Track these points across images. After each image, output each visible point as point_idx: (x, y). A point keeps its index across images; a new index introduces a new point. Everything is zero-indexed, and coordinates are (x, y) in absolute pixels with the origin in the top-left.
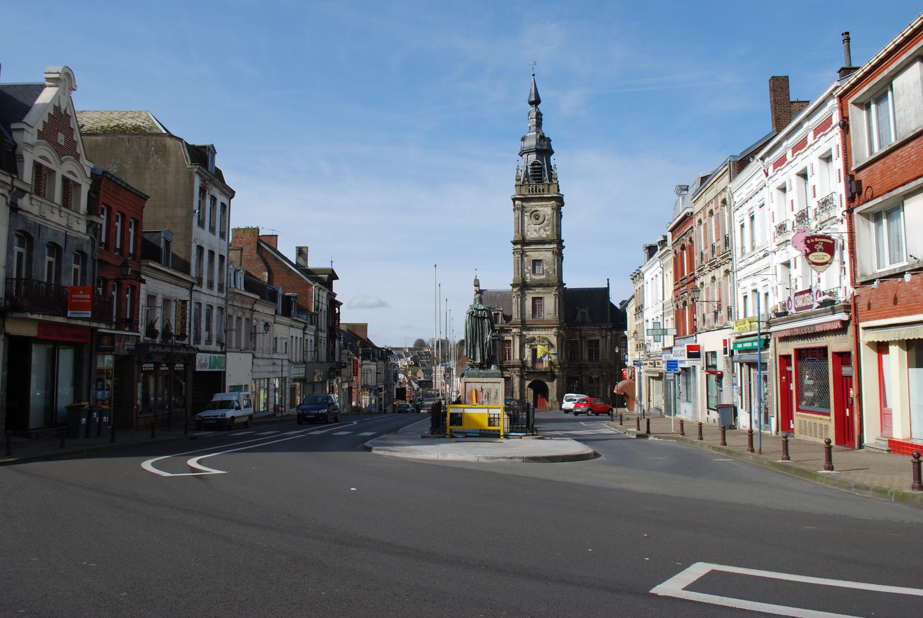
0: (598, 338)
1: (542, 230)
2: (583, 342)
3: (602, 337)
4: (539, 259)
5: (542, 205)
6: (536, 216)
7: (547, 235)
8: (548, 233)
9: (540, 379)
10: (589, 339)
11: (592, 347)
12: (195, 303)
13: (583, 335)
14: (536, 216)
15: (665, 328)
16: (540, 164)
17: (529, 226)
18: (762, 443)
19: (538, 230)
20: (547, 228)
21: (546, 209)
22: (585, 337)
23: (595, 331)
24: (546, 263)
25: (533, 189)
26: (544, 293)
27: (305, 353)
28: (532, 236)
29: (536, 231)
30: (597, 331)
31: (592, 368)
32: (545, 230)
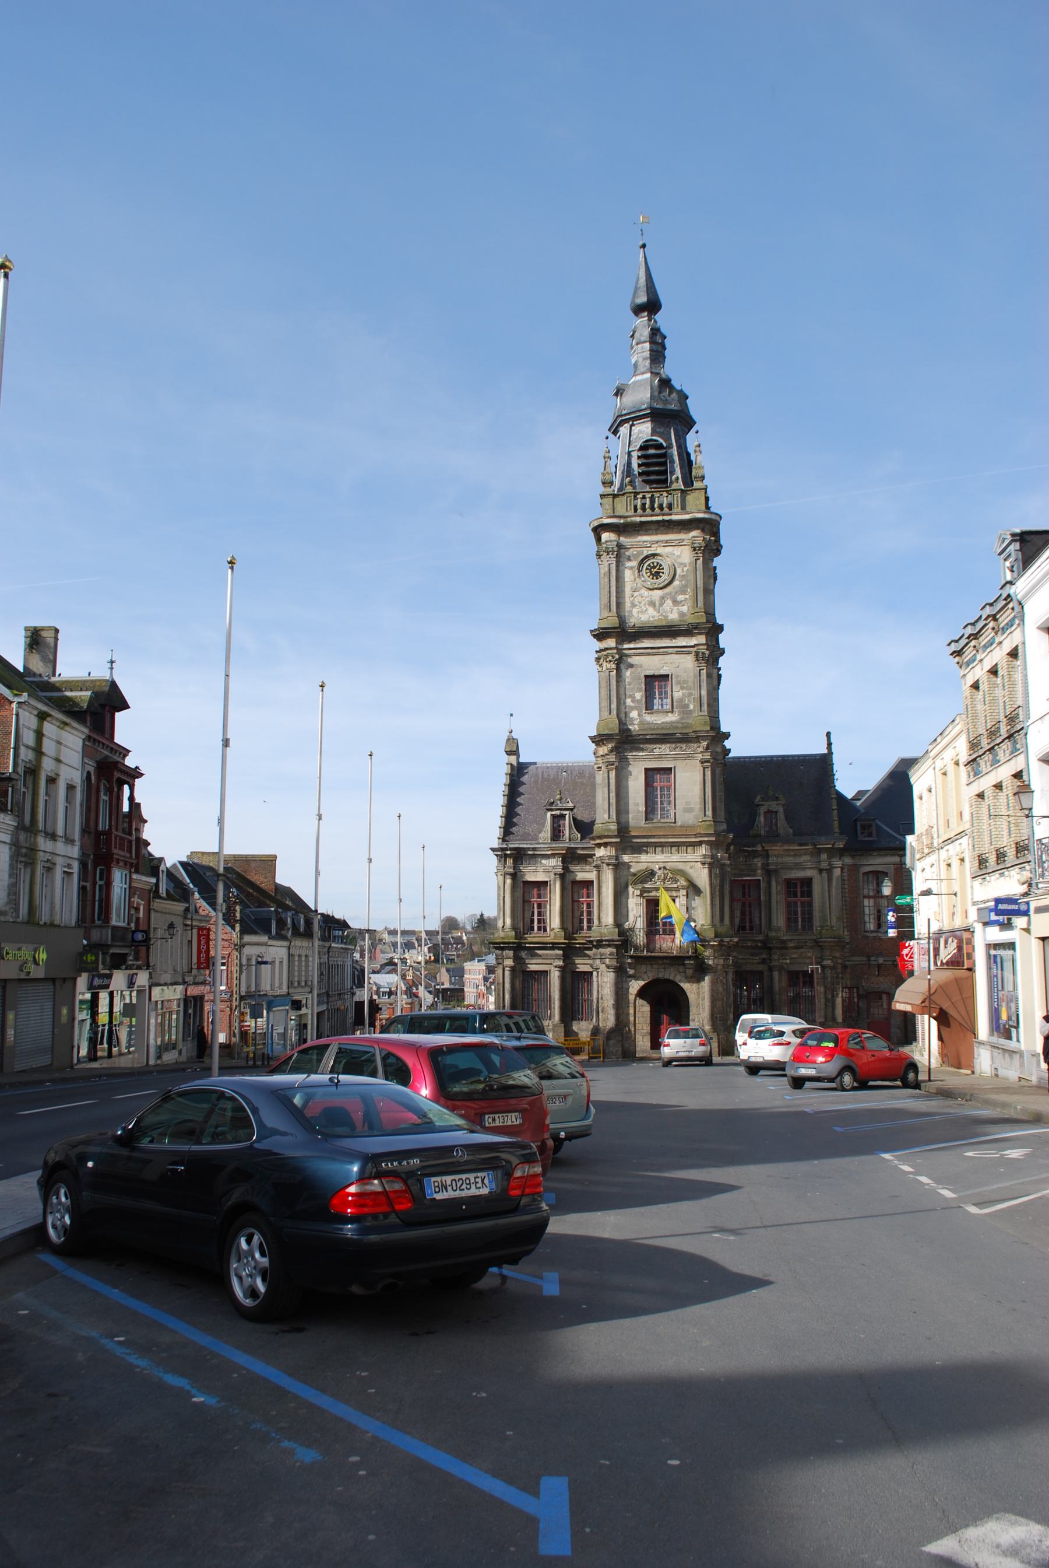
0: (808, 873)
2: (774, 883)
3: (821, 871)
6: (651, 567)
7: (682, 614)
9: (667, 977)
10: (787, 877)
11: (795, 896)
17: (636, 594)
20: (681, 597)
22: (776, 871)
23: (800, 855)
26: (675, 758)
28: (644, 618)
31: (796, 948)
32: (675, 602)
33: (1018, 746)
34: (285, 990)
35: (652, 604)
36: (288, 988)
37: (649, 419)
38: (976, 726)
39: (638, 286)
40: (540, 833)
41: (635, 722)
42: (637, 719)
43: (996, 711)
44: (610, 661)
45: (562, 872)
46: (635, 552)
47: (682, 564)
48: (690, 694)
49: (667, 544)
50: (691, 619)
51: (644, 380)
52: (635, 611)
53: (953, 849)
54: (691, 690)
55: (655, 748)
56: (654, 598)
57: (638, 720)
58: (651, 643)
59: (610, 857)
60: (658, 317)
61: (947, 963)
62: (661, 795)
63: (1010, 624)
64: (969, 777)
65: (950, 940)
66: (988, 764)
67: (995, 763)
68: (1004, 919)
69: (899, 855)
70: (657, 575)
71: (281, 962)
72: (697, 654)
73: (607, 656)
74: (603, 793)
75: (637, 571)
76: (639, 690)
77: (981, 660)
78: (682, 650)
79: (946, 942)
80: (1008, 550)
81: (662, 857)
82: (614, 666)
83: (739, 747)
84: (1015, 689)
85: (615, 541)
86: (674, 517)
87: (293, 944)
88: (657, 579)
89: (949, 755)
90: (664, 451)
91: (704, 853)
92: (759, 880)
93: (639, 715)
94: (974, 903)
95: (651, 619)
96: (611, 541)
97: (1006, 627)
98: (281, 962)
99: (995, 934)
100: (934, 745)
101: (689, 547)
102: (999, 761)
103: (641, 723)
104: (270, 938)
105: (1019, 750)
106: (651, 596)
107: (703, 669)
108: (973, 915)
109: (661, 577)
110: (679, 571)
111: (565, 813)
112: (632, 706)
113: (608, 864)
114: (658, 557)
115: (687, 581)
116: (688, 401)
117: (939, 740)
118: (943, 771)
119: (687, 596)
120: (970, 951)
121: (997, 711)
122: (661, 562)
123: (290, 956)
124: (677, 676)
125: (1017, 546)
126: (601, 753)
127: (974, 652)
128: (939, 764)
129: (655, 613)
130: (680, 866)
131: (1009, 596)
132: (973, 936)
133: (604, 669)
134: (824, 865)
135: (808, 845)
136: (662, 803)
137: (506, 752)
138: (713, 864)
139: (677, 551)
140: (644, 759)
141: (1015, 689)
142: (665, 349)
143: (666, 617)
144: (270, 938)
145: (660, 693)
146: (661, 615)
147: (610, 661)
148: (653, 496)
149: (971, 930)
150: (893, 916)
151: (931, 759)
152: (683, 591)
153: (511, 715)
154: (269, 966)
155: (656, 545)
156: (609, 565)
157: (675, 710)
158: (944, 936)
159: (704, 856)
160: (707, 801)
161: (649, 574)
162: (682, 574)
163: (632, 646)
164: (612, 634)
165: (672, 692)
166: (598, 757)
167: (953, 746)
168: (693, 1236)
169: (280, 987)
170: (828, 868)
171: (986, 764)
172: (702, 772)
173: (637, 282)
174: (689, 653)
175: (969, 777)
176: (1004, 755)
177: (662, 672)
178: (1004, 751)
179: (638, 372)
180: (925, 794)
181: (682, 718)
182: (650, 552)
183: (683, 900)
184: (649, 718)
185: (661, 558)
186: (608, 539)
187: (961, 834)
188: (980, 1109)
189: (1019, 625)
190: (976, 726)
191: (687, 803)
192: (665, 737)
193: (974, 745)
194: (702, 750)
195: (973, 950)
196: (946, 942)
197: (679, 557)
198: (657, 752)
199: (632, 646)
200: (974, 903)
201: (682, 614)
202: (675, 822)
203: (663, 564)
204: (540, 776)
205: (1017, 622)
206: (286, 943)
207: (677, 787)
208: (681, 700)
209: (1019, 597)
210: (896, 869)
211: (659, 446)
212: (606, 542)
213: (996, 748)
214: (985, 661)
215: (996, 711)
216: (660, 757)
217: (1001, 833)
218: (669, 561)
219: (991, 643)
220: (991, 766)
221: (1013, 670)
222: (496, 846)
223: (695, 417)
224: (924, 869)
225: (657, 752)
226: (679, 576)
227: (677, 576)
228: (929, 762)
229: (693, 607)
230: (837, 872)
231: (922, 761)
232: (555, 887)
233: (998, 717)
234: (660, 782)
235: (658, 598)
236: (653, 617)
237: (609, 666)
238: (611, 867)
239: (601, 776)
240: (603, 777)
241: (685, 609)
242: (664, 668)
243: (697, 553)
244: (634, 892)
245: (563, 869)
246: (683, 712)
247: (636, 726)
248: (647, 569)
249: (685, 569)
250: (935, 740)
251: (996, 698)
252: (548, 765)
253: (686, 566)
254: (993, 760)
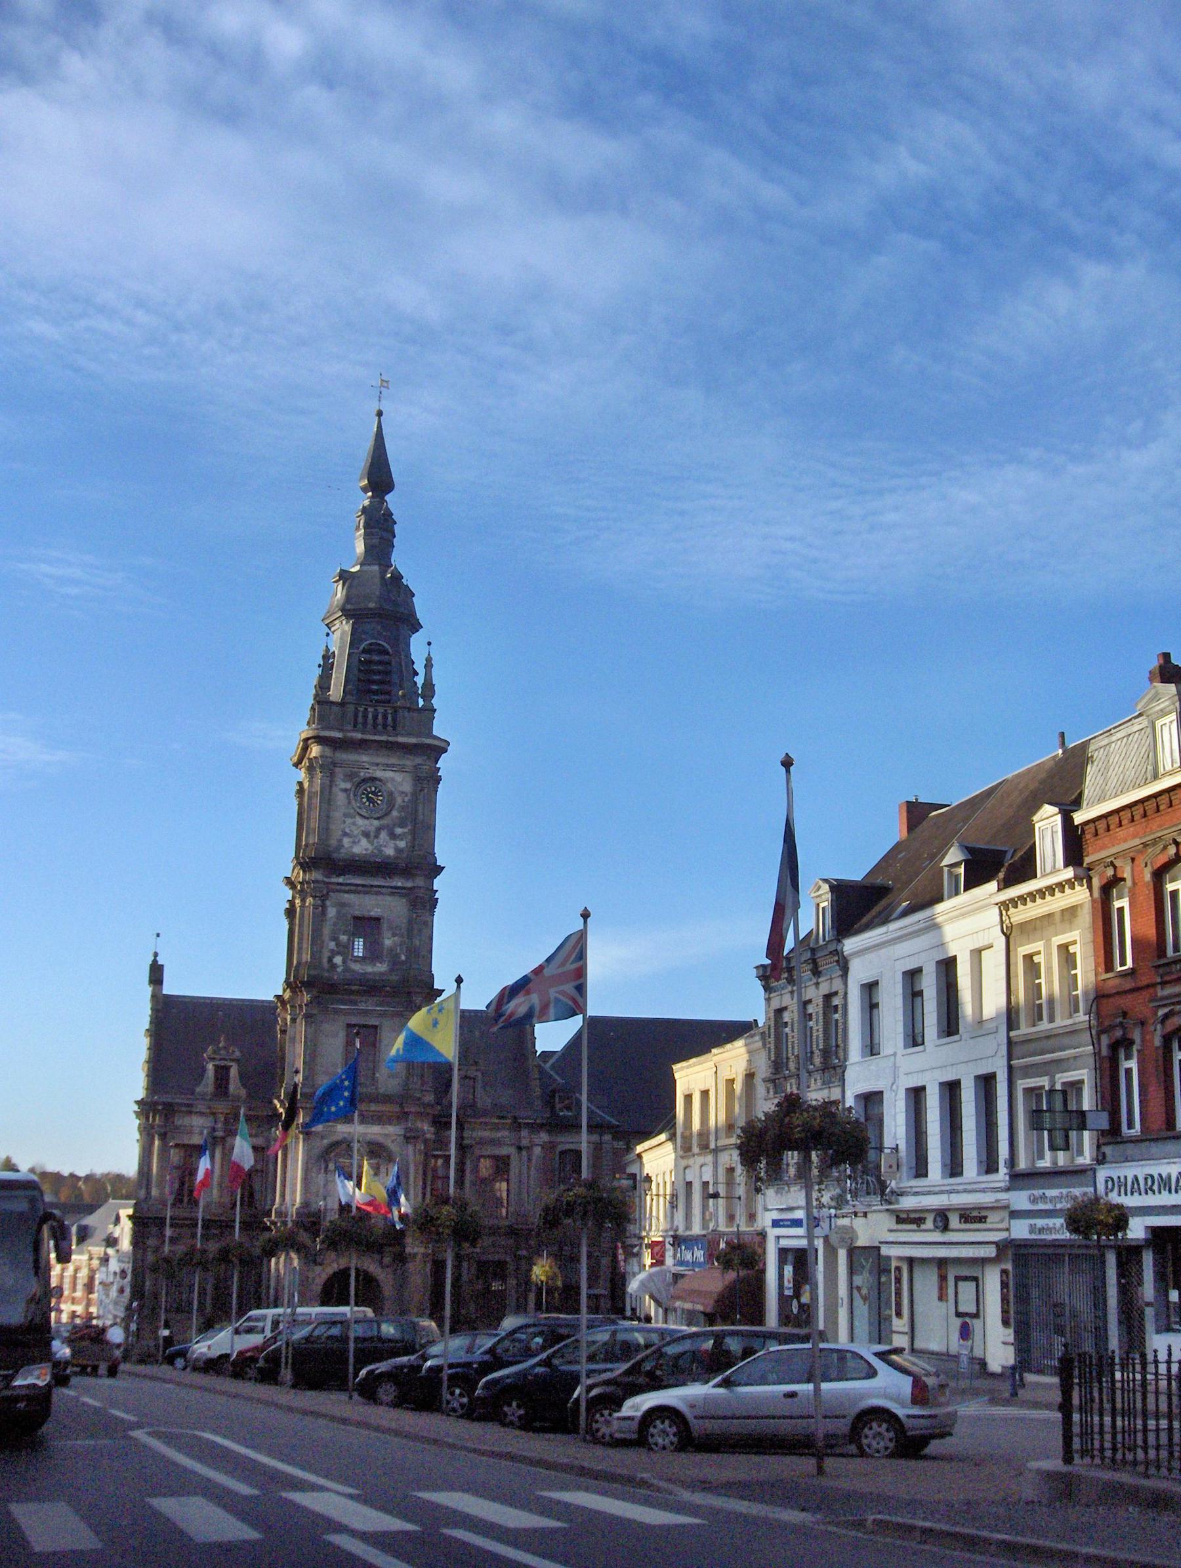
0: (504, 1151)
1: (384, 835)
3: (520, 1148)
4: (372, 914)
5: (387, 765)
6: (366, 787)
7: (398, 850)
8: (402, 844)
12: (666, 1321)
13: (466, 1142)
14: (366, 787)
15: (709, 1158)
16: (386, 653)
18: (960, 1297)
19: (372, 834)
20: (399, 831)
21: (398, 777)
23: (498, 1129)
24: (390, 928)
25: (375, 718)
26: (382, 1015)
27: (668, 1339)
28: (357, 850)
29: (366, 835)
30: (506, 1133)
32: (393, 836)
52: (346, 841)
86: (401, 739)
93: (344, 962)
103: (347, 969)
119: (406, 830)
129: (370, 848)
134: (525, 1142)
140: (347, 1013)
142: (394, 537)
153: (158, 935)
163: (341, 880)
168: (916, 1302)
170: (529, 1145)
182: (368, 775)
188: (564, 1487)
199: (341, 880)
201: (398, 850)
208: (391, 950)
216: (365, 1013)
223: (420, 614)
230: (537, 1151)
236: (366, 850)
249: (406, 799)
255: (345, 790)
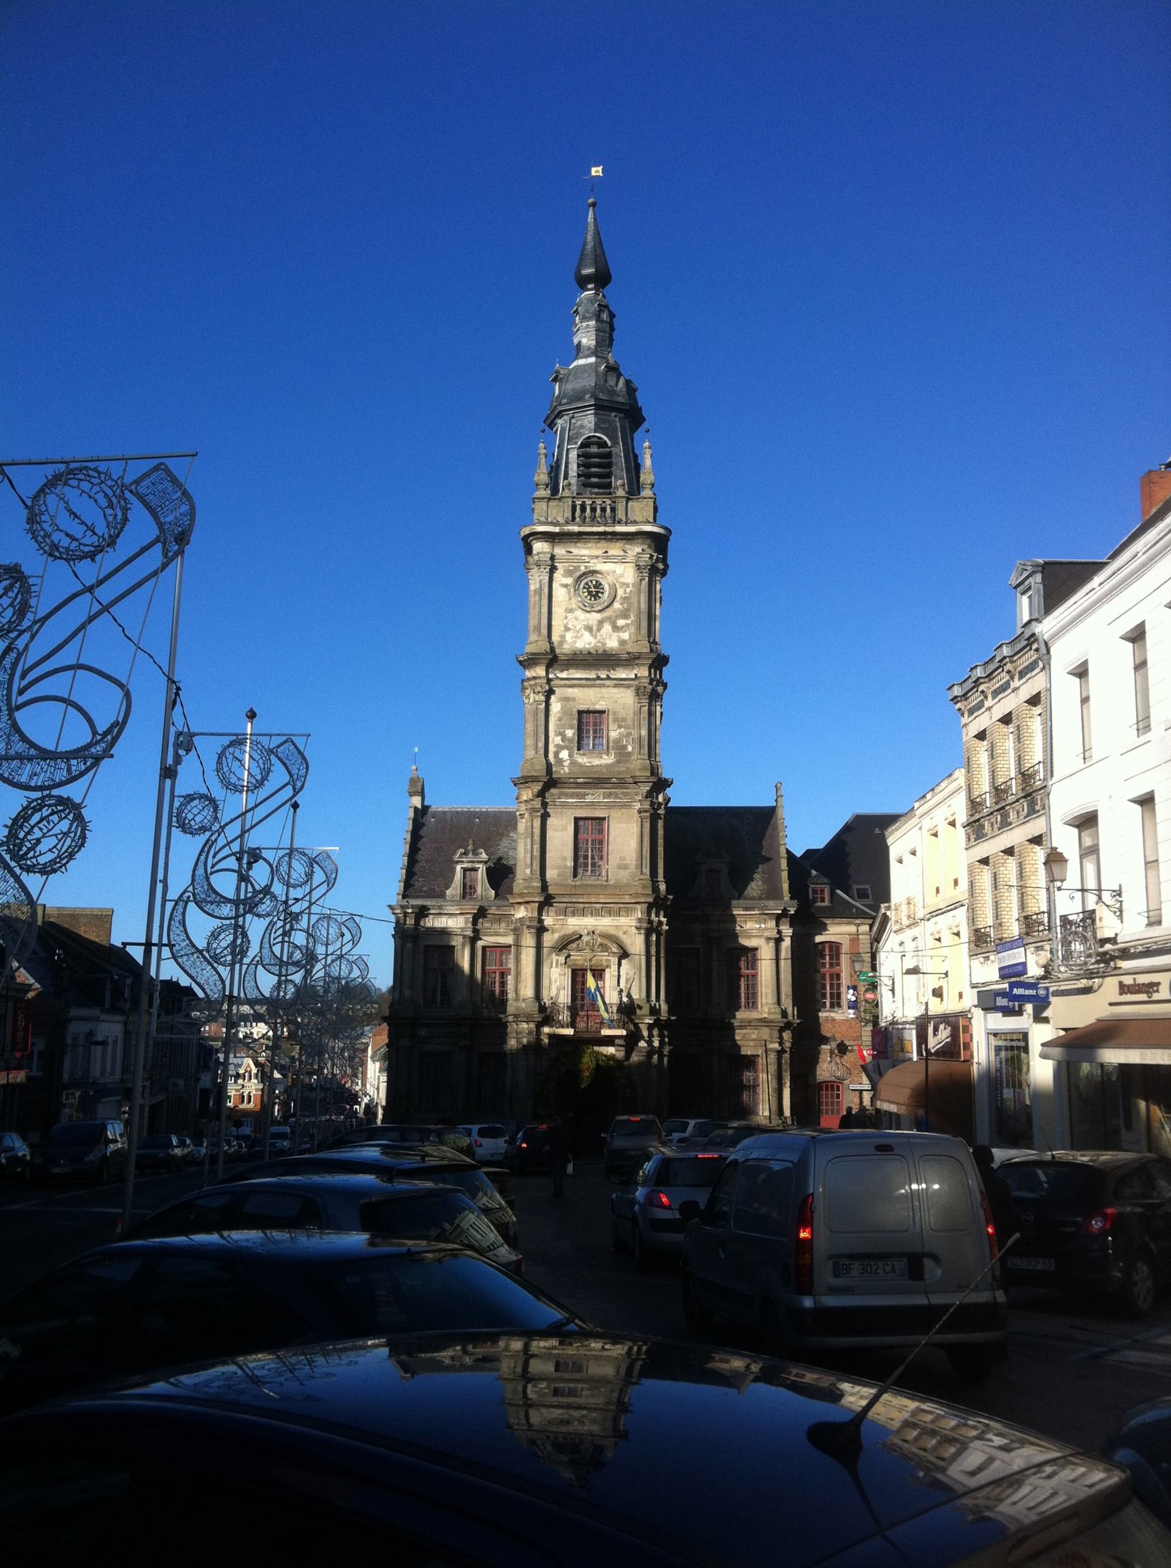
7: (623, 642)
17: (570, 615)
19: (595, 628)
20: (621, 622)
26: (610, 806)
32: (616, 628)
33: (1037, 808)
34: (118, 1075)
35: (589, 629)
36: (122, 1074)
37: (592, 412)
38: (979, 783)
39: (585, 252)
40: (447, 889)
41: (565, 764)
42: (566, 760)
43: (1005, 766)
44: (539, 692)
45: (472, 935)
46: (571, 568)
47: (624, 584)
48: (629, 734)
49: (607, 557)
50: (632, 648)
51: (588, 364)
52: (569, 636)
53: (944, 922)
54: (629, 728)
55: (587, 795)
56: (591, 623)
57: (569, 762)
58: (586, 674)
59: (531, 919)
60: (608, 289)
61: (937, 1053)
62: (592, 848)
63: (1032, 667)
64: (969, 840)
65: (942, 1027)
66: (995, 826)
67: (1005, 824)
68: (1014, 1005)
69: (855, 924)
70: (596, 596)
71: (115, 1042)
72: (638, 690)
73: (536, 684)
74: (526, 845)
75: (572, 590)
76: (571, 727)
77: (989, 709)
78: (620, 683)
79: (936, 1030)
80: (1027, 583)
81: (624, 921)
82: (543, 698)
83: (680, 797)
84: (1032, 742)
85: (548, 553)
87: (130, 1018)
88: (595, 599)
89: (939, 817)
90: (609, 450)
91: (640, 916)
92: (699, 949)
93: (570, 755)
94: (973, 986)
95: (587, 646)
96: (544, 553)
97: (1025, 671)
98: (115, 1042)
99: (998, 1022)
100: (922, 802)
101: (634, 565)
102: (1011, 824)
104: (102, 1012)
105: (1039, 811)
106: (588, 619)
107: (645, 706)
108: (971, 998)
109: (600, 598)
110: (620, 592)
111: (477, 866)
112: (562, 746)
113: (528, 927)
114: (598, 575)
115: (629, 604)
116: (636, 393)
117: (929, 796)
118: (932, 832)
119: (629, 622)
120: (968, 1040)
121: (1008, 766)
122: (601, 580)
123: (127, 1033)
124: (615, 713)
125: (1038, 577)
126: (525, 798)
127: (982, 697)
128: (927, 823)
130: (612, 931)
131: (1033, 635)
132: (971, 1024)
133: (531, 701)
135: (754, 910)
136: (593, 858)
137: (409, 793)
138: (650, 930)
139: (619, 569)
141: (1032, 742)
143: (604, 644)
144: (102, 1012)
145: (595, 731)
146: (599, 642)
147: (539, 692)
148: (594, 502)
149: (969, 1016)
150: (853, 995)
151: (916, 818)
152: (625, 614)
154: (99, 1048)
155: (596, 561)
156: (541, 581)
157: (610, 751)
158: (932, 1022)
159: (640, 920)
160: (644, 857)
161: (586, 594)
162: (624, 596)
164: (543, 661)
165: (608, 730)
166: (520, 802)
167: (948, 804)
169: (113, 1072)
171: (992, 826)
172: (640, 823)
173: (584, 248)
174: (629, 687)
175: (969, 840)
176: (1018, 817)
177: (598, 707)
178: (1018, 813)
179: (581, 355)
180: (907, 858)
181: (618, 762)
183: (614, 971)
184: (582, 760)
185: (600, 576)
186: (541, 551)
187: (955, 906)
189: (1044, 668)
190: (979, 783)
191: (622, 858)
192: (598, 781)
193: (974, 805)
194: (640, 798)
195: (971, 1040)
196: (936, 1030)
197: (622, 576)
198: (589, 799)
200: (973, 986)
201: (623, 642)
202: (607, 881)
203: (603, 582)
204: (449, 822)
205: (1041, 664)
206: (121, 1018)
207: (610, 839)
209: (1045, 637)
210: (852, 940)
211: (602, 444)
212: (538, 553)
213: (1007, 808)
214: (994, 710)
215: (1005, 766)
216: (592, 805)
217: (1009, 906)
218: (610, 579)
219: (1004, 688)
220: (999, 829)
221: (1031, 720)
222: (394, 903)
224: (903, 943)
225: (589, 799)
226: (621, 597)
227: (618, 598)
228: (914, 821)
229: (637, 635)
231: (902, 819)
232: (463, 952)
233: (1008, 773)
234: (592, 834)
235: (595, 622)
237: (537, 698)
238: (532, 930)
239: (524, 825)
240: (526, 826)
241: (625, 636)
242: (601, 702)
243: (641, 573)
244: (557, 960)
245: (473, 932)
246: (620, 754)
247: (566, 769)
248: (584, 588)
249: (628, 590)
250: (924, 796)
251: (1007, 751)
252: (458, 810)
253: (628, 587)
254: (1002, 821)
255: (566, 586)
